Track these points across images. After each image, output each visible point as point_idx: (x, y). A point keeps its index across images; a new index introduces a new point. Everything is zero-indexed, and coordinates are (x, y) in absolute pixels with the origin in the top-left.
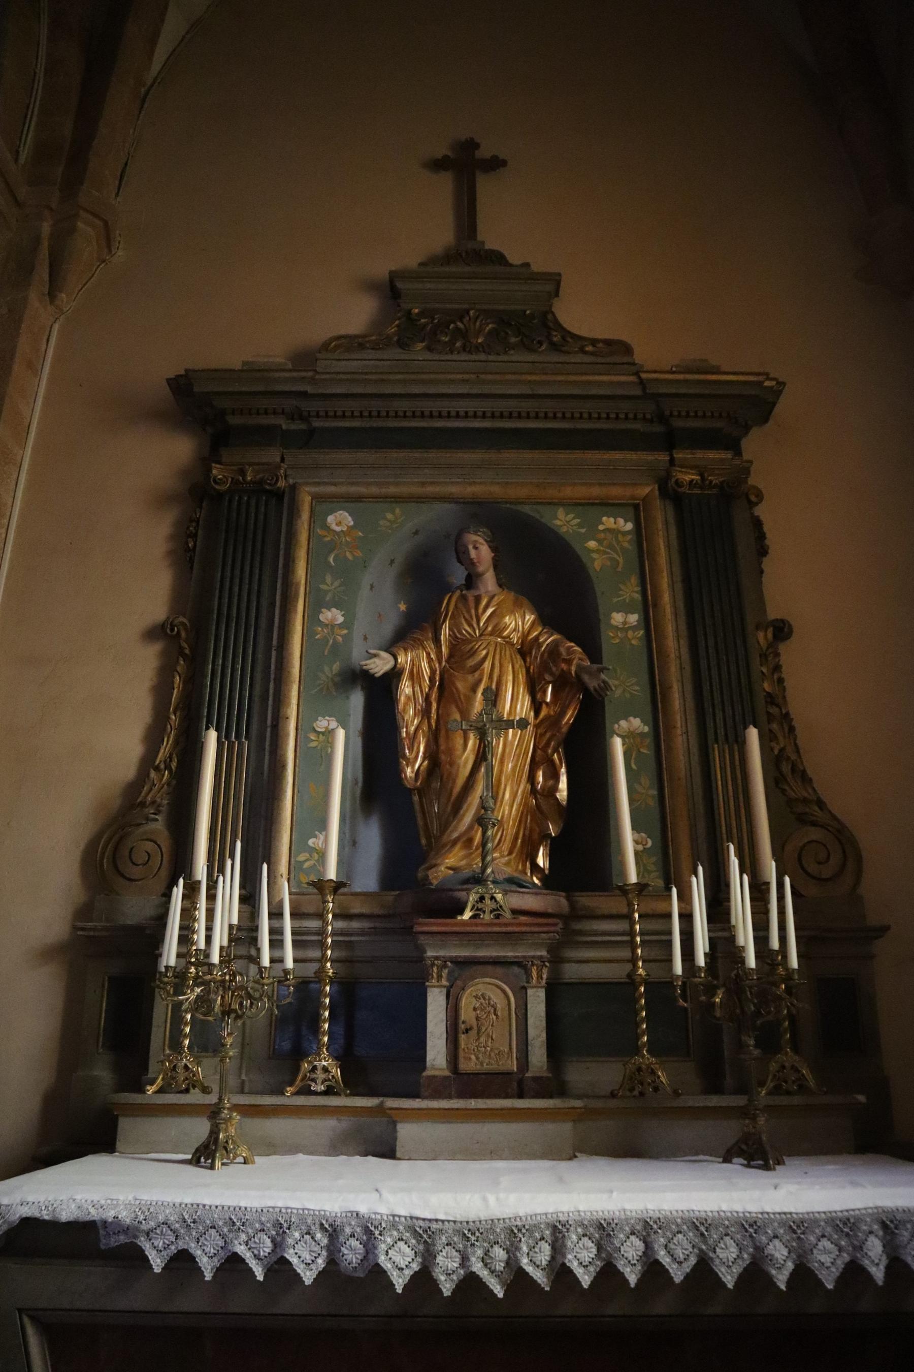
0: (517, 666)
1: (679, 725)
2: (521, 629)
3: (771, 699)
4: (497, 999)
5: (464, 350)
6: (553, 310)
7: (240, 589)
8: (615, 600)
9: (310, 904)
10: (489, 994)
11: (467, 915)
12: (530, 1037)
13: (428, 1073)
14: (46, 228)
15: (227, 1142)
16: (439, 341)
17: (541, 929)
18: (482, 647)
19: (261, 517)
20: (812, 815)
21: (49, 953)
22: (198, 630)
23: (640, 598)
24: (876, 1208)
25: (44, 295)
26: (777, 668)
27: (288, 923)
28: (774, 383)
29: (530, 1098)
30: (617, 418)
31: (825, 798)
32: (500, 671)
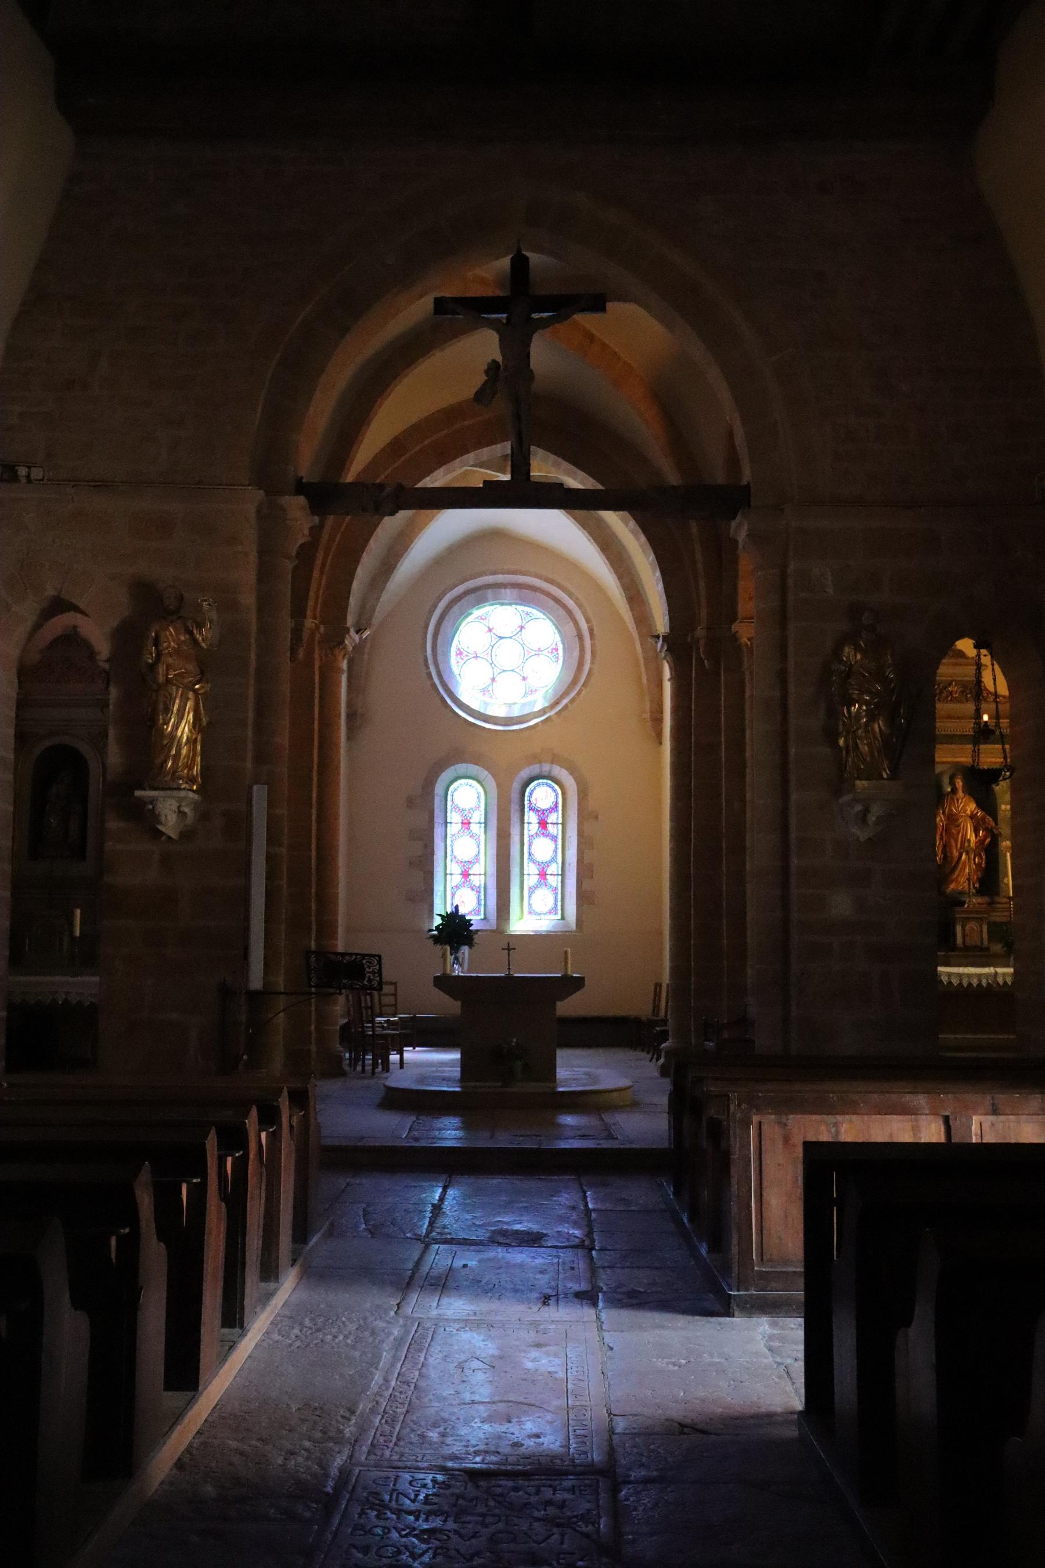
4: (975, 928)
11: (966, 906)
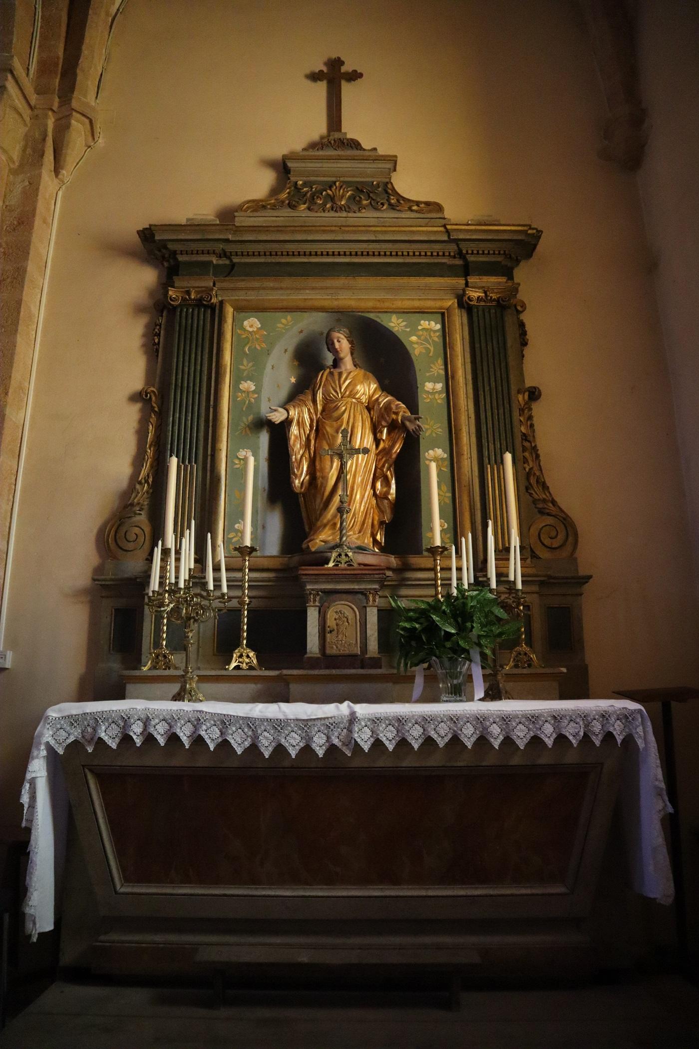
0: (365, 417)
1: (466, 453)
2: (367, 394)
3: (525, 437)
4: (348, 612)
5: (332, 210)
6: (392, 181)
7: (189, 369)
8: (428, 374)
9: (237, 562)
10: (343, 610)
11: (331, 564)
12: (368, 635)
13: (308, 655)
14: (51, 123)
15: (191, 691)
16: (316, 204)
17: (375, 572)
18: (342, 405)
19: (201, 322)
20: (548, 509)
21: (79, 593)
22: (163, 395)
23: (444, 373)
24: (551, 709)
25: (51, 171)
26: (530, 418)
27: (224, 574)
28: (535, 231)
29: (369, 668)
30: (432, 255)
31: (557, 499)
32: (354, 420)
